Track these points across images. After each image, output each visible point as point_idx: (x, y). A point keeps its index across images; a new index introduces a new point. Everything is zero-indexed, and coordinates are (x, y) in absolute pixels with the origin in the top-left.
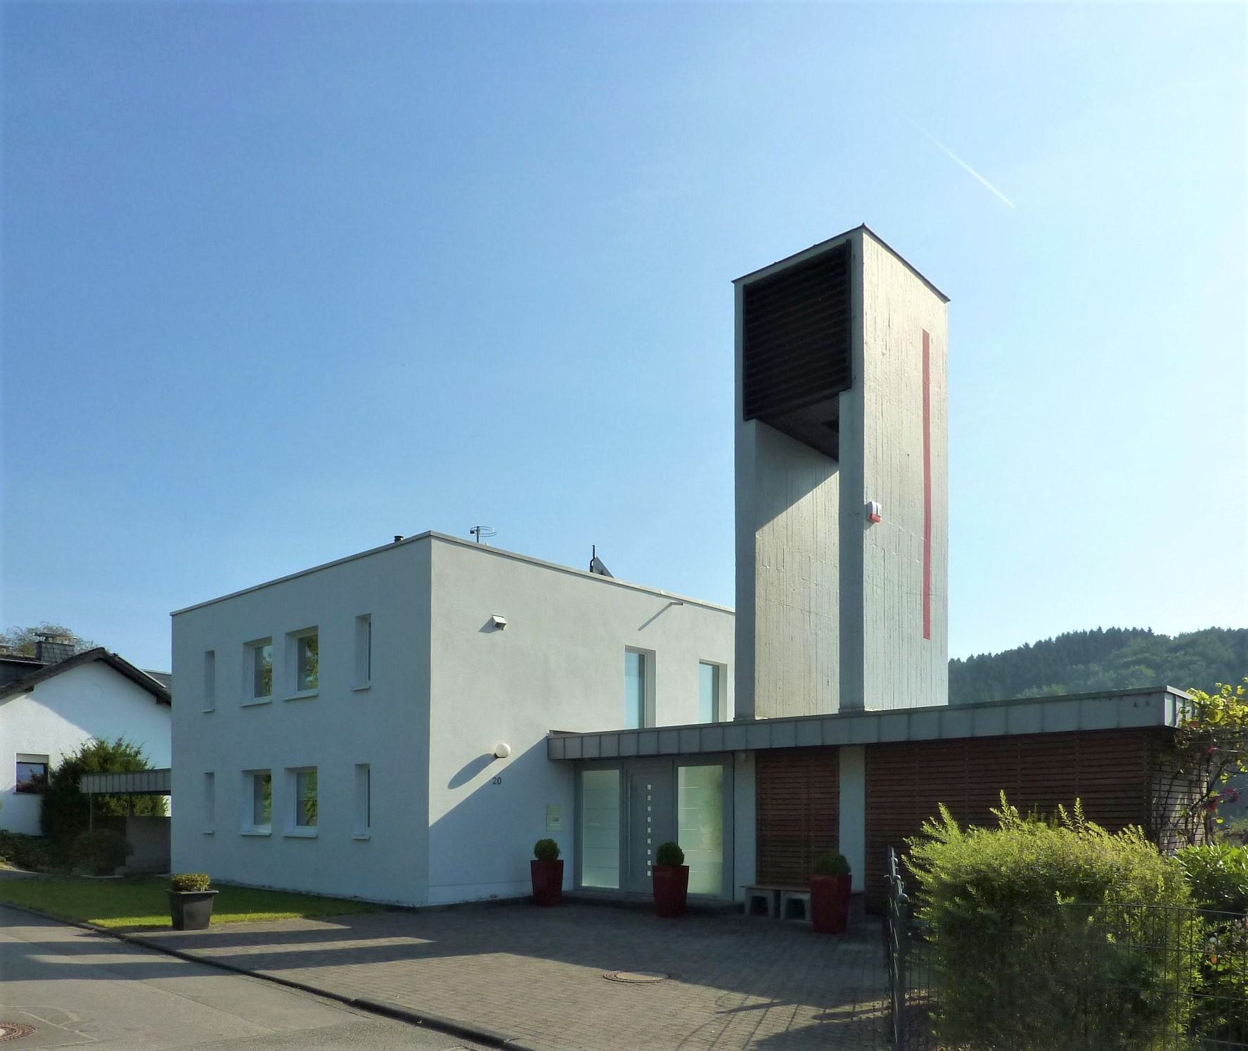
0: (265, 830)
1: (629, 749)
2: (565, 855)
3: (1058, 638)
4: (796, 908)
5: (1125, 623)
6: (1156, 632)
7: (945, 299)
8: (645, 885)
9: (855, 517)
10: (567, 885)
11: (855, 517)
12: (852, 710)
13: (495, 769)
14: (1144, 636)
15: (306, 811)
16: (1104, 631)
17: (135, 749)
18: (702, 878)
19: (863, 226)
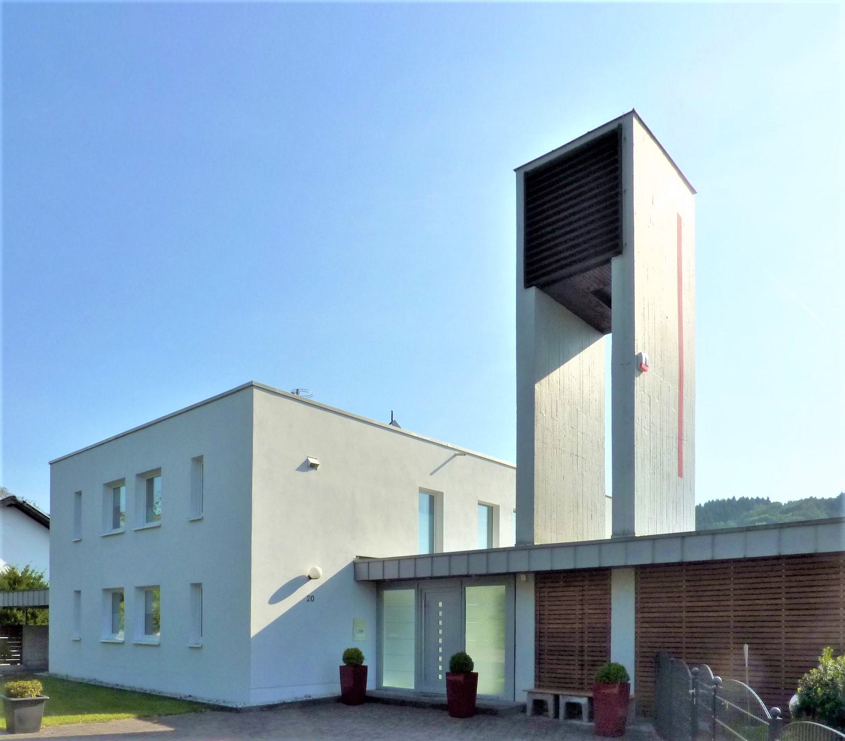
0: (120, 637)
1: (424, 571)
2: (368, 662)
3: (706, 504)
4: (574, 711)
5: (751, 493)
6: (772, 500)
7: (693, 191)
8: (439, 688)
9: (627, 366)
10: (370, 686)
11: (627, 366)
12: (624, 536)
13: (308, 588)
14: (767, 502)
15: (152, 623)
16: (737, 499)
17: (39, 574)
18: (488, 684)
19: (633, 111)
